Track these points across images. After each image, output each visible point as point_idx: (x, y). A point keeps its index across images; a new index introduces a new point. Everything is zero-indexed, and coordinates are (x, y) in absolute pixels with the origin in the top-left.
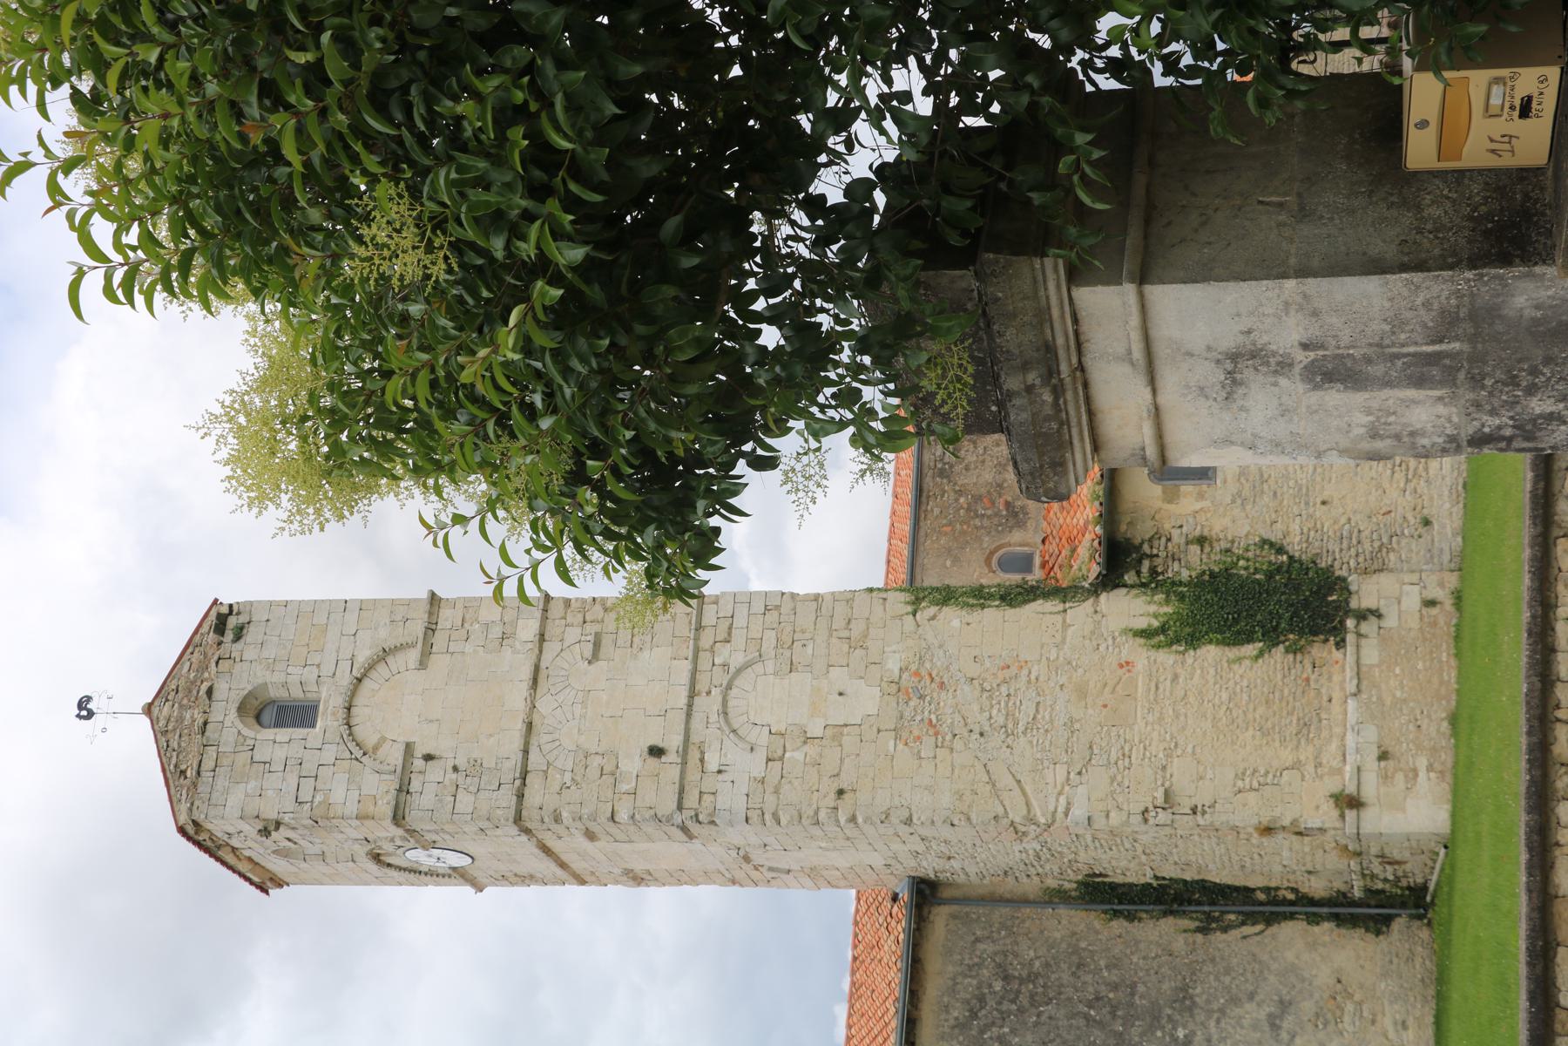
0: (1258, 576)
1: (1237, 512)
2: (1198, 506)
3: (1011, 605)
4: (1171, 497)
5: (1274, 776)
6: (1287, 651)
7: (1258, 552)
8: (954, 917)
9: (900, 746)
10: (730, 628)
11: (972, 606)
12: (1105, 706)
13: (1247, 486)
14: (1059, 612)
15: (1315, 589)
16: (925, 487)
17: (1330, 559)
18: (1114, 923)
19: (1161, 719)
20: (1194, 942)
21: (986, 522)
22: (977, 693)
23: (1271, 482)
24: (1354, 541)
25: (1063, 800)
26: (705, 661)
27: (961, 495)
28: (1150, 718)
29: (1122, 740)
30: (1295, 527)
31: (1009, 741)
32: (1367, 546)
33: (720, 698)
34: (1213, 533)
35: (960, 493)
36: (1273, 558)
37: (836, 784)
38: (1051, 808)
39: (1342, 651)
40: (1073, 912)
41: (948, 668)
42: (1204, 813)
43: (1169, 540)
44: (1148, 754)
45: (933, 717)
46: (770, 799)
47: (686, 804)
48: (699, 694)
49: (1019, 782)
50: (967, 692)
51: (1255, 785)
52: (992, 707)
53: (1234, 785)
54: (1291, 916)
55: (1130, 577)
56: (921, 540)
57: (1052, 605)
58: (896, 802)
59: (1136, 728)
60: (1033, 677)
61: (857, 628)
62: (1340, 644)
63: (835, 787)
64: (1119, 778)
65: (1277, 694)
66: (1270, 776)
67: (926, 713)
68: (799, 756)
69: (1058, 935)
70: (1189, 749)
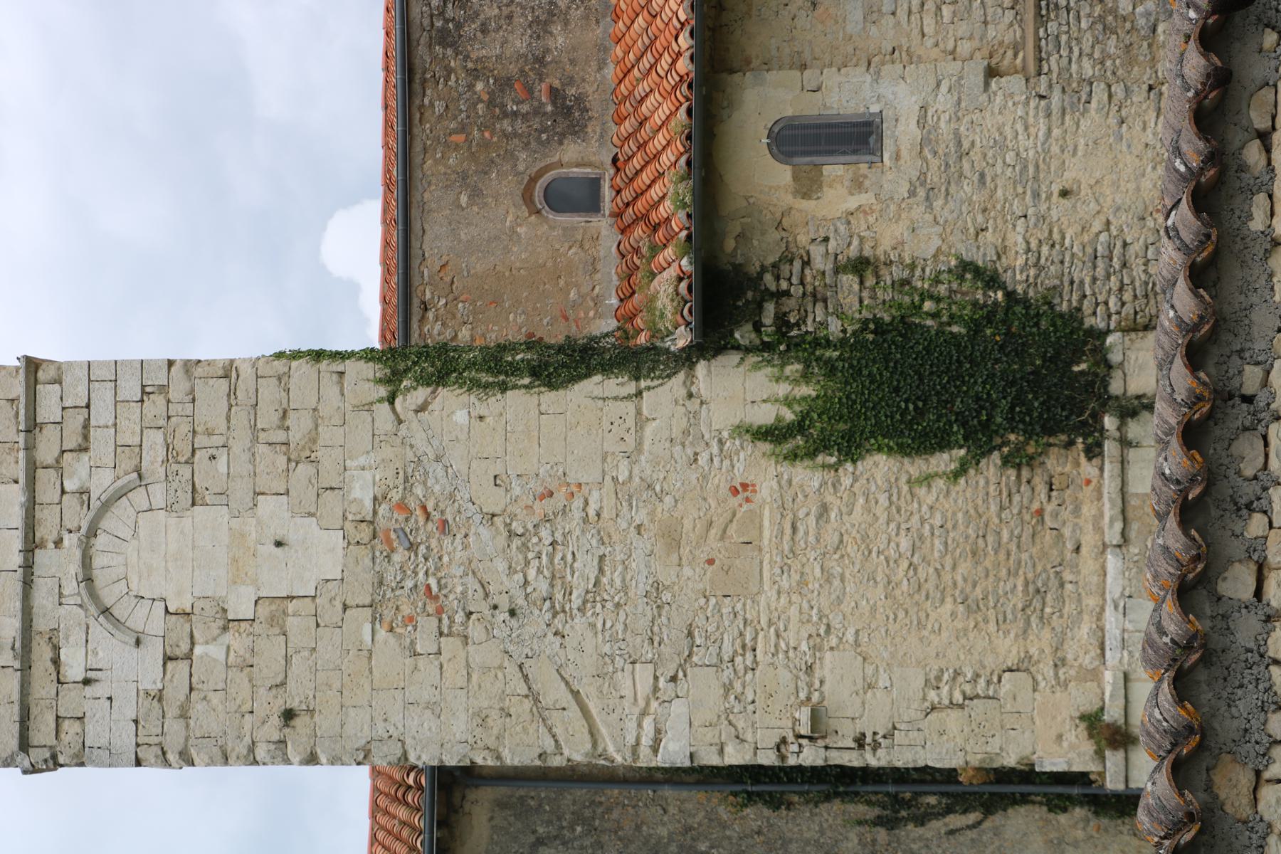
0: (955, 329)
1: (918, 211)
2: (852, 203)
3: (552, 386)
4: (808, 186)
5: (989, 683)
6: (1006, 461)
7: (955, 286)
8: (501, 805)
9: (382, 633)
10: (86, 425)
11: (487, 386)
12: (711, 562)
13: (935, 163)
14: (628, 397)
15: (1050, 352)
16: (417, 61)
17: (1075, 297)
18: (749, 811)
19: (802, 583)
20: (874, 841)
21: (521, 127)
22: (502, 540)
23: (976, 155)
24: (1116, 263)
25: (648, 724)
26: (46, 479)
27: (477, 78)
28: (785, 584)
29: (740, 620)
30: (1016, 239)
31: (558, 623)
32: (1138, 271)
33: (78, 554)
34: (880, 252)
35: (475, 74)
36: (979, 296)
37: (280, 702)
38: (631, 739)
39: (1096, 461)
40: (685, 794)
41: (451, 496)
42: (876, 746)
43: (807, 263)
44: (783, 645)
45: (433, 582)
46: (174, 727)
47: (36, 738)
48: (42, 545)
49: (576, 694)
50: (486, 538)
51: (958, 697)
52: (527, 563)
53: (924, 699)
54: (1024, 800)
55: (743, 335)
56: (417, 160)
57: (618, 385)
58: (380, 729)
59: (763, 600)
60: (591, 512)
61: (299, 426)
62: (1094, 451)
63: (279, 706)
64: (738, 685)
65: (990, 539)
66: (982, 682)
67: (421, 575)
68: (217, 652)
69: (663, 832)
70: (850, 637)
